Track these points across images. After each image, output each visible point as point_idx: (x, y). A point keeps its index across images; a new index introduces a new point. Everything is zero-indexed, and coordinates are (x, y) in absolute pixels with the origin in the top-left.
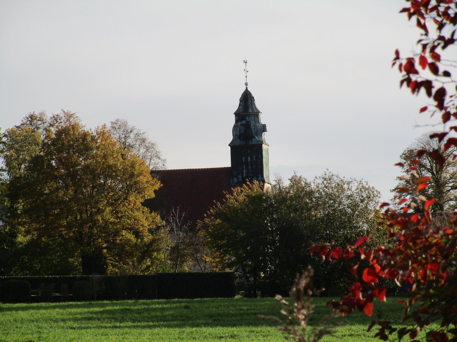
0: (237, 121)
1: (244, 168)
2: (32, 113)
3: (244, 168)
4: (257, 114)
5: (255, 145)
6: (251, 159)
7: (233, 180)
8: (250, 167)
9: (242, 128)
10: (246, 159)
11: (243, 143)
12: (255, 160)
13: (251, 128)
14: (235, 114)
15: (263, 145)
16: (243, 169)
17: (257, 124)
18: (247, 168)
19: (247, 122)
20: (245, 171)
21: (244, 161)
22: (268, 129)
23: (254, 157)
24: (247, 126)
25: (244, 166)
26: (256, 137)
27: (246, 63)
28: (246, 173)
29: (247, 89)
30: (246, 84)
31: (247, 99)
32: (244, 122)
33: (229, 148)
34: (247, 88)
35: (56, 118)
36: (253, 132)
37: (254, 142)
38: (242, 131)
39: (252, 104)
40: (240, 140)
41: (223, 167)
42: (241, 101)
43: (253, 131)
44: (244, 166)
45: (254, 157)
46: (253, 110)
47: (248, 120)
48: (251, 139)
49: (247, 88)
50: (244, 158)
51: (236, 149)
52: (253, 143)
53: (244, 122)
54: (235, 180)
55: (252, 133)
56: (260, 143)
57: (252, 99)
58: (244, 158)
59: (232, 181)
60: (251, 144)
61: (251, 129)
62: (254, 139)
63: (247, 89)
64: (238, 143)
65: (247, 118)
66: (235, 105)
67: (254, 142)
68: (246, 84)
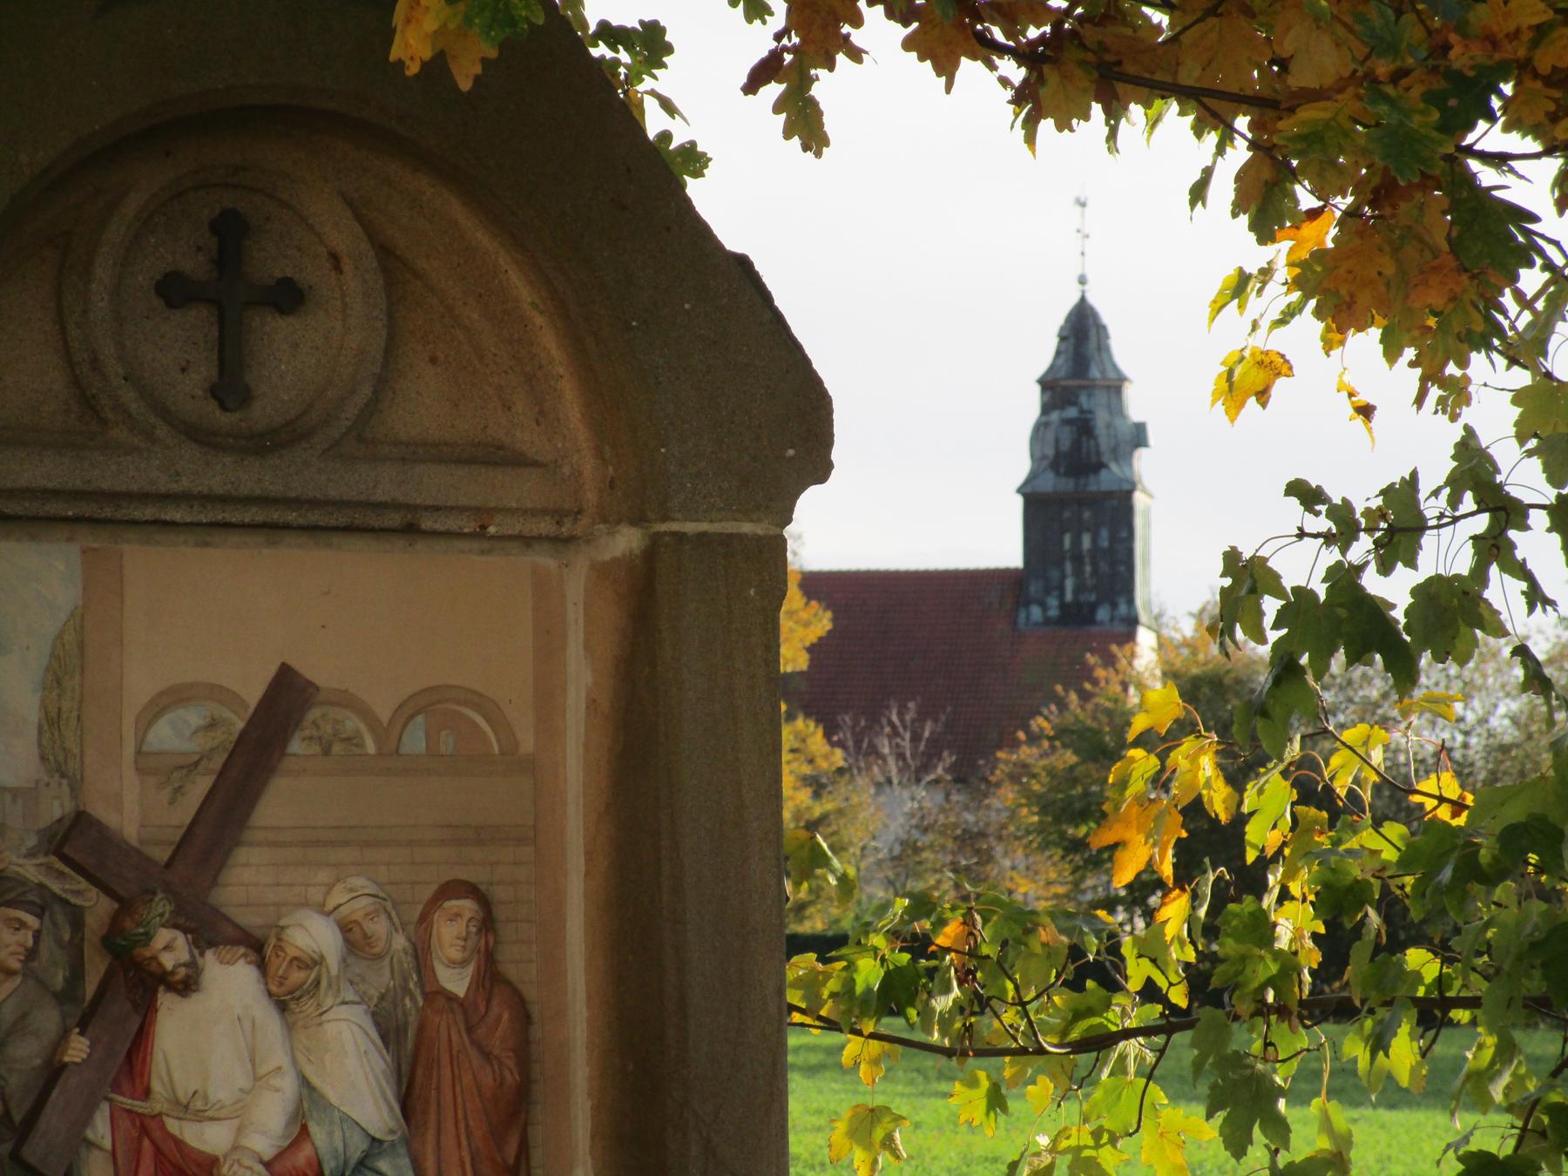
0: (1046, 409)
4: (1115, 385)
6: (1094, 541)
8: (1088, 569)
10: (1077, 542)
11: (1067, 485)
16: (1063, 577)
17: (1118, 422)
18: (1078, 573)
19: (1082, 411)
20: (1069, 584)
22: (1152, 435)
23: (1104, 533)
24: (1084, 427)
25: (1069, 567)
27: (1083, 205)
28: (1077, 590)
29: (1083, 299)
30: (1082, 280)
31: (1082, 332)
32: (1072, 412)
37: (1104, 481)
38: (1066, 445)
40: (1057, 473)
42: (1063, 338)
43: (1104, 443)
44: (1069, 567)
45: (1104, 533)
46: (1103, 372)
51: (1040, 509)
53: (1072, 412)
56: (1126, 487)
58: (1105, 544)
61: (1095, 438)
62: (1104, 473)
63: (1083, 299)
64: (1049, 483)
65: (1083, 399)
67: (1104, 481)
68: (1082, 280)
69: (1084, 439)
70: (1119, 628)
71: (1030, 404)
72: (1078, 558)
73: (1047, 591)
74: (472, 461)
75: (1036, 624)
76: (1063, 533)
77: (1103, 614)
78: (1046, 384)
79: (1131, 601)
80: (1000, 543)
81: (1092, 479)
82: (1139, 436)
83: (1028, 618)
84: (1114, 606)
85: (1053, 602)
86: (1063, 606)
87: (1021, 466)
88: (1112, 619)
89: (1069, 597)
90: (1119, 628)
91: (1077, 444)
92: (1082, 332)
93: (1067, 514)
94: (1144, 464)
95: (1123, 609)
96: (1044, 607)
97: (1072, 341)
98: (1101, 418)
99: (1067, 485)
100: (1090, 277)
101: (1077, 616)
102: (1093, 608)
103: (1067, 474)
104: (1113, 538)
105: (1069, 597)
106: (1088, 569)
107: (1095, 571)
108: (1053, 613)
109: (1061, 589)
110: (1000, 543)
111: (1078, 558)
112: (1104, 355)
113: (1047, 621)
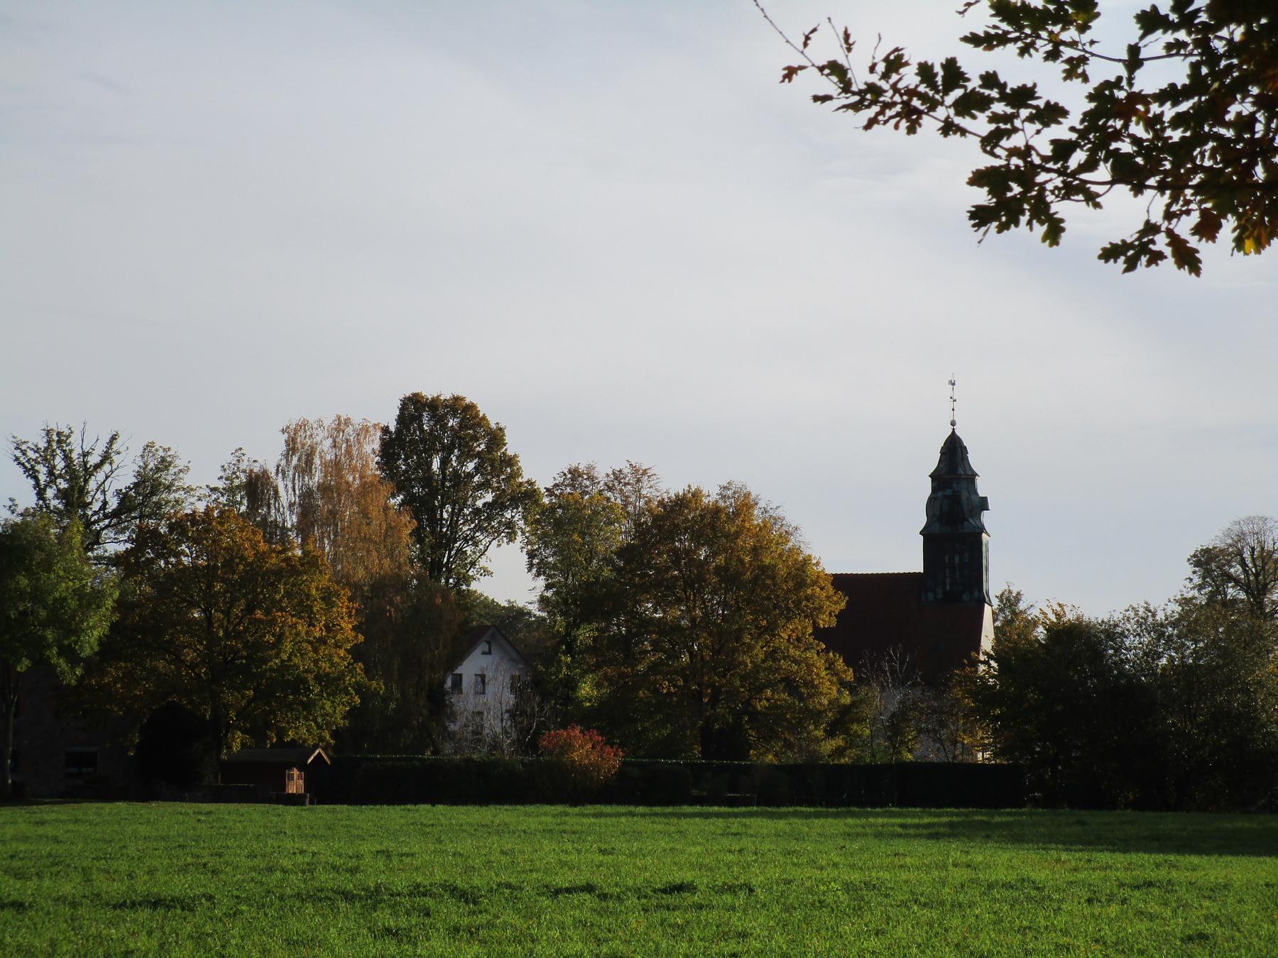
2: (1030, 85)
4: (971, 477)
17: (973, 497)
20: (948, 581)
23: (966, 555)
24: (955, 500)
29: (953, 432)
31: (954, 450)
32: (949, 492)
45: (966, 555)
51: (932, 539)
63: (953, 432)
64: (937, 528)
77: (966, 597)
78: (933, 476)
82: (983, 504)
87: (922, 520)
89: (948, 588)
92: (954, 450)
94: (986, 518)
95: (976, 594)
98: (964, 495)
105: (948, 588)
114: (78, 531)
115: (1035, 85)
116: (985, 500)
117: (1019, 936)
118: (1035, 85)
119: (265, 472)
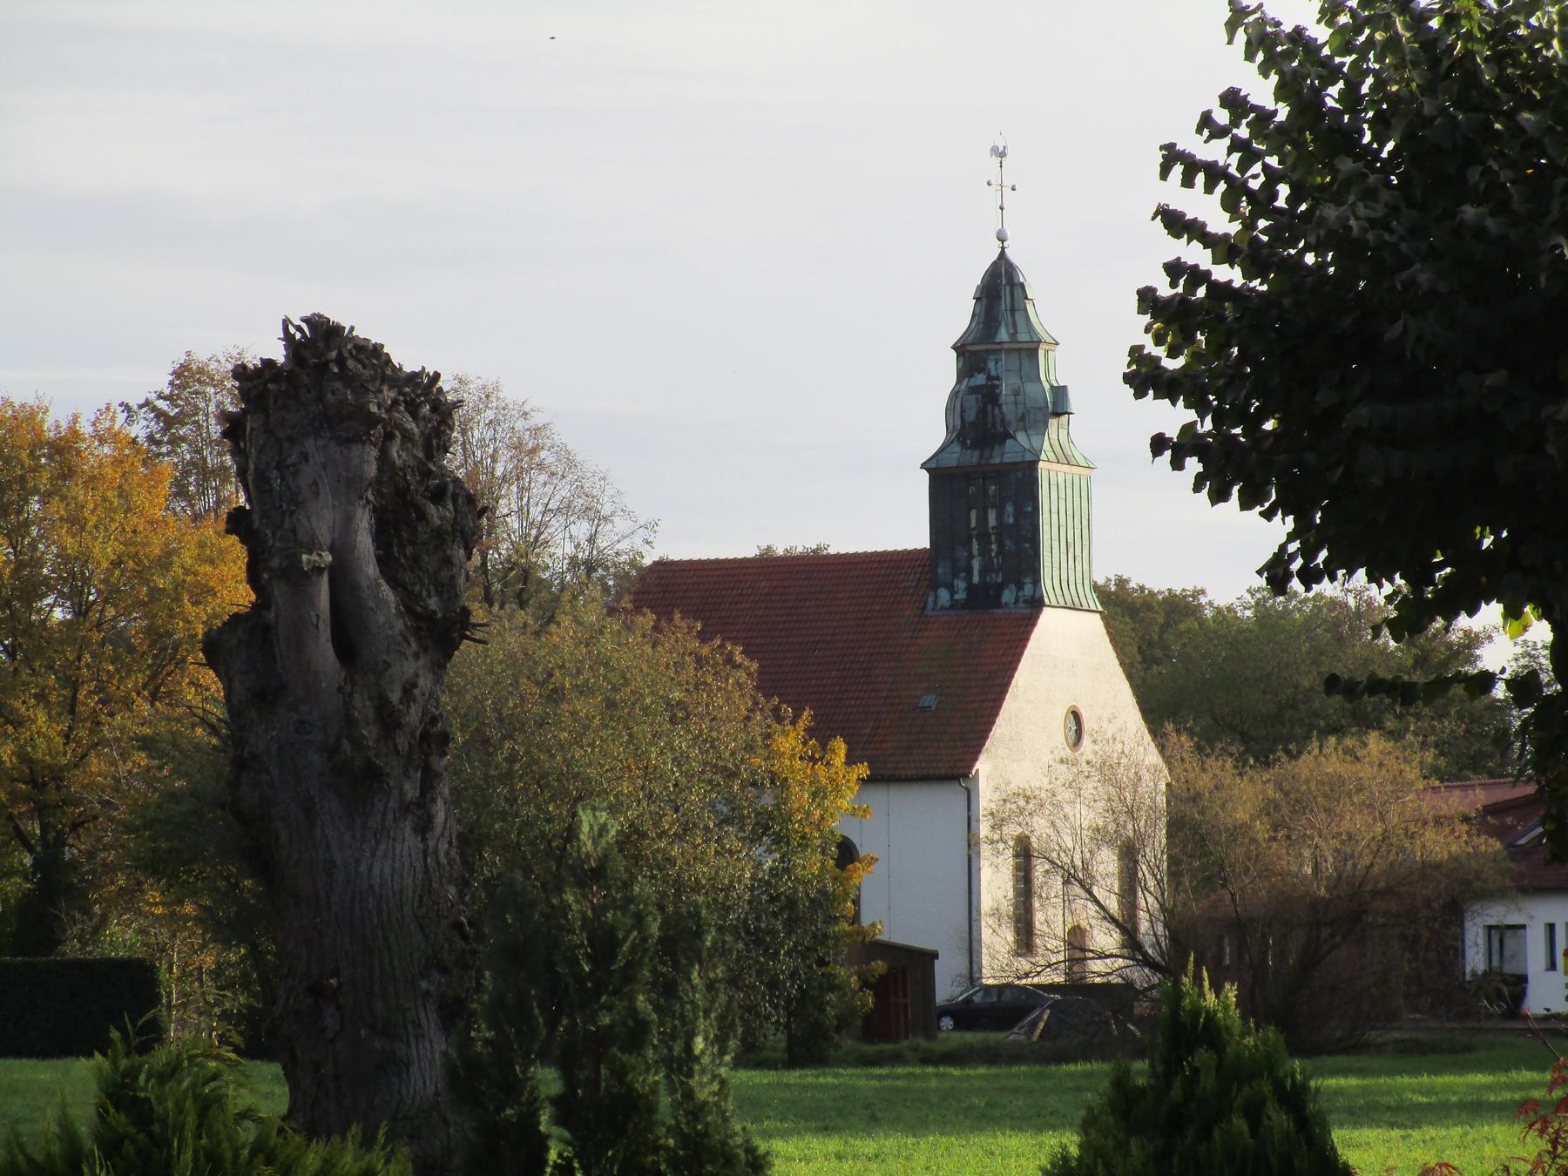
0: (959, 381)
1: (975, 552)
2: (182, 359)
3: (975, 552)
4: (1029, 351)
5: (1014, 465)
6: (1000, 517)
7: (936, 597)
8: (994, 547)
9: (972, 400)
10: (983, 518)
11: (973, 457)
12: (1011, 521)
13: (1003, 399)
14: (954, 347)
15: (1041, 464)
16: (971, 557)
17: (1030, 388)
18: (985, 552)
19: (990, 378)
20: (976, 564)
21: (973, 524)
22: (1074, 401)
23: (1009, 509)
24: (989, 395)
25: (975, 546)
26: (1021, 437)
27: (1002, 155)
28: (983, 573)
29: (1002, 255)
31: (1000, 291)
32: (980, 379)
33: (925, 475)
34: (1003, 248)
35: (23, 406)
36: (1010, 417)
37: (1011, 452)
38: (971, 415)
39: (1013, 310)
40: (964, 445)
41: (695, 558)
42: (978, 299)
43: (1008, 409)
44: (975, 546)
45: (1009, 509)
46: (1013, 335)
47: (993, 373)
48: (1002, 441)
49: (1003, 248)
50: (973, 514)
51: (949, 483)
52: (1006, 460)
53: (980, 379)
54: (944, 595)
55: (1003, 421)
56: (1029, 457)
57: (1018, 291)
58: (973, 514)
59: (931, 599)
60: (997, 461)
61: (1000, 407)
62: (1009, 442)
63: (1002, 255)
64: (952, 460)
65: (991, 365)
66: (959, 316)
67: (1011, 452)
69: (989, 407)
70: (1023, 610)
71: (944, 374)
72: (984, 537)
73: (955, 575)
74: (969, 819)
75: (942, 608)
76: (970, 510)
77: (1008, 596)
79: (1037, 581)
80: (899, 522)
81: (997, 449)
83: (935, 602)
84: (1020, 586)
85: (961, 584)
86: (970, 588)
88: (1017, 600)
89: (976, 579)
90: (1023, 610)
91: (982, 412)
92: (1000, 291)
93: (972, 489)
95: (1028, 590)
96: (952, 590)
97: (984, 301)
99: (973, 457)
100: (1009, 234)
101: (983, 598)
102: (999, 588)
103: (973, 447)
104: (1018, 513)
105: (976, 579)
106: (994, 547)
107: (1000, 551)
108: (961, 596)
109: (969, 570)
110: (899, 522)
111: (984, 537)
112: (1019, 317)
113: (954, 605)
114: (1409, 82)
115: (188, 354)
116: (1060, 392)
117: (205, 618)
118: (188, 354)
119: (74, 434)
